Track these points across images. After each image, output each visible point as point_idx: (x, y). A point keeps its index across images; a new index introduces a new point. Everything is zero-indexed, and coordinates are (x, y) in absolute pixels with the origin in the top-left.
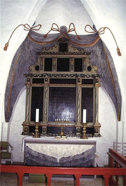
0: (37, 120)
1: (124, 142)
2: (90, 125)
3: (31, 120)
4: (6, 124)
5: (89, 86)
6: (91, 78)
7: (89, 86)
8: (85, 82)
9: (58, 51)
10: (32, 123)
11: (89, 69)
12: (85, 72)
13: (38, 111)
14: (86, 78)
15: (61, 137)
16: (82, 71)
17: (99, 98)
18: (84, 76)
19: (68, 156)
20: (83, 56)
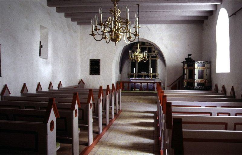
0: (134, 72)
1: (92, 33)
2: (154, 74)
3: (131, 72)
4: (120, 74)
5: (154, 59)
6: (155, 55)
7: (154, 59)
8: (152, 57)
9: (140, 37)
10: (132, 74)
11: (154, 52)
12: (152, 53)
13: (134, 69)
14: (153, 55)
15: (185, 74)
16: (151, 53)
17: (157, 44)
18: (152, 55)
19: (93, 119)
20: (152, 46)
